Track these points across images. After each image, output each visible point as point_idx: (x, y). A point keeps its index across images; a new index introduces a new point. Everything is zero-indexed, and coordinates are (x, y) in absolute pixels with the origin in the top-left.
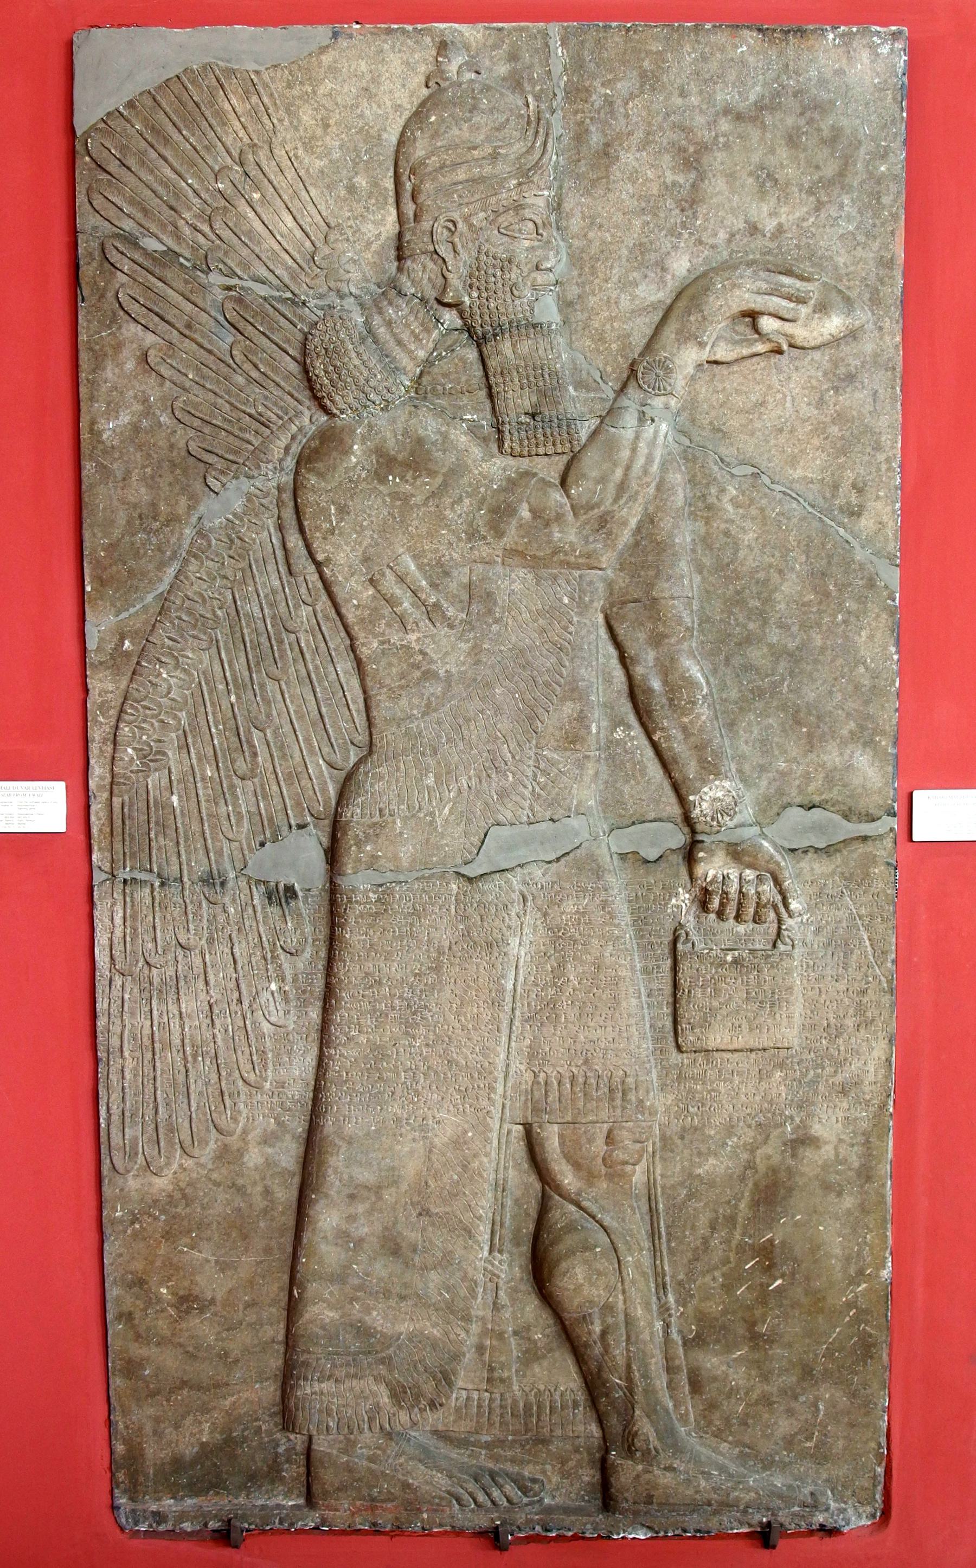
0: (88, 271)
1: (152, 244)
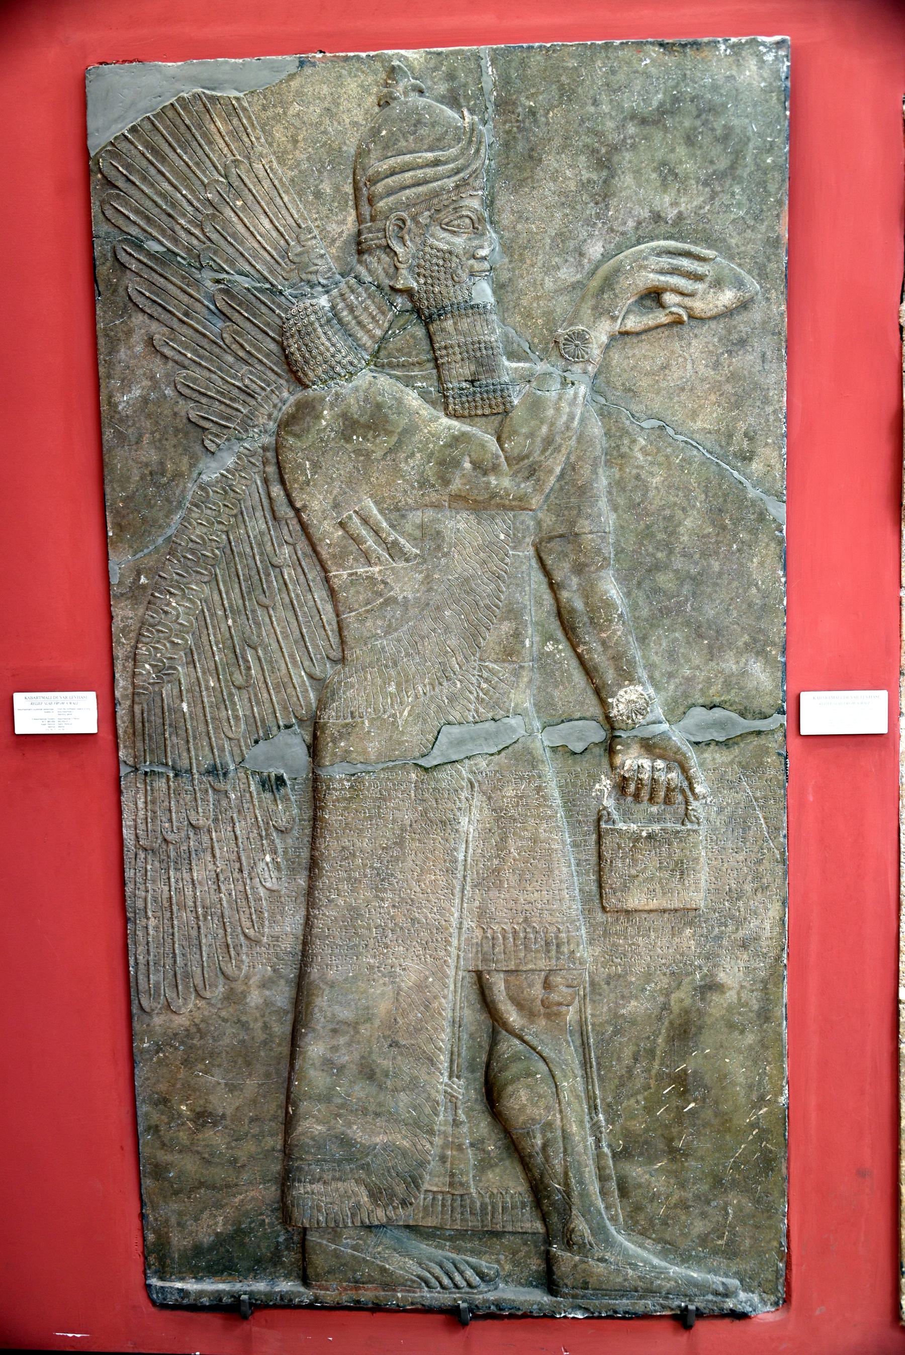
0: (103, 270)
1: (154, 247)
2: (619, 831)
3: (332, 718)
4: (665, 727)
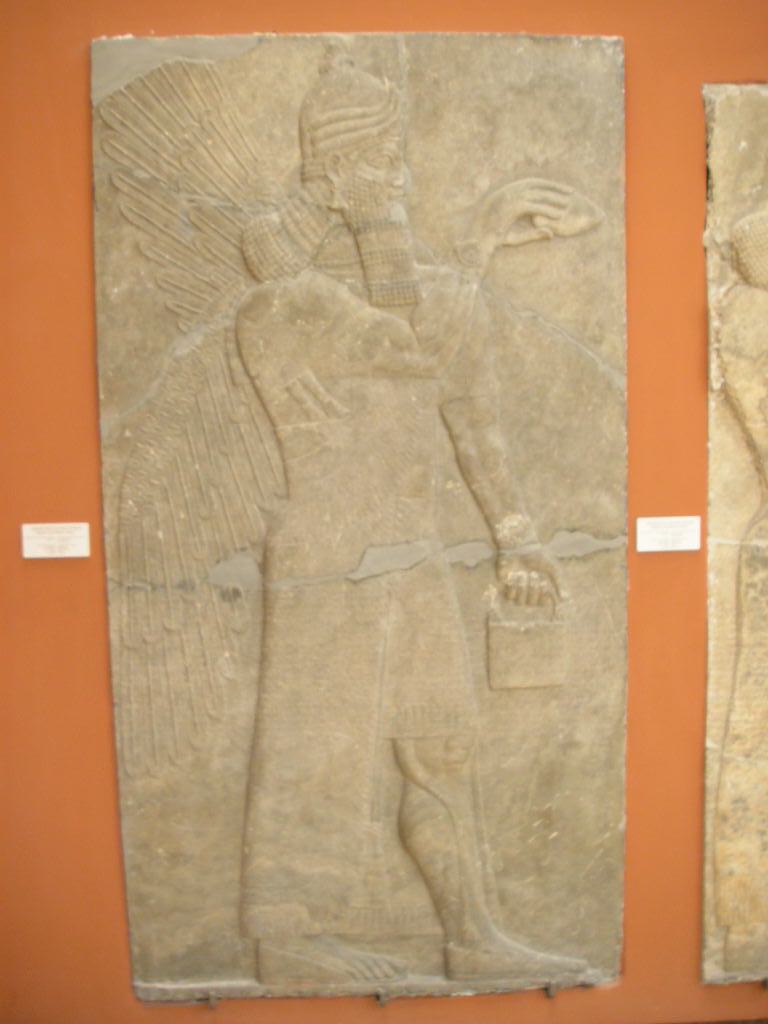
0: (101, 192)
1: (141, 174)
2: (503, 628)
3: (279, 542)
4: (537, 547)
